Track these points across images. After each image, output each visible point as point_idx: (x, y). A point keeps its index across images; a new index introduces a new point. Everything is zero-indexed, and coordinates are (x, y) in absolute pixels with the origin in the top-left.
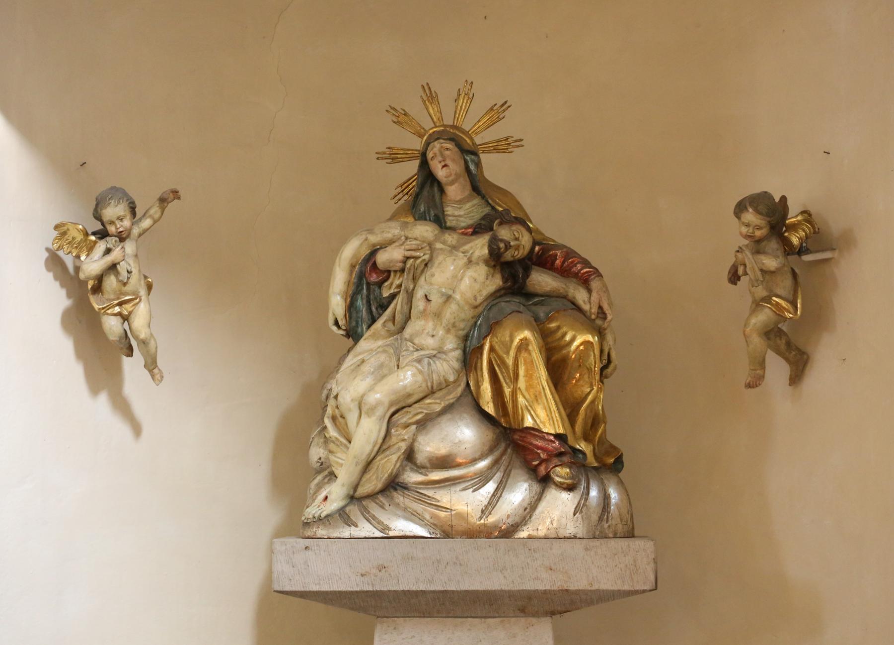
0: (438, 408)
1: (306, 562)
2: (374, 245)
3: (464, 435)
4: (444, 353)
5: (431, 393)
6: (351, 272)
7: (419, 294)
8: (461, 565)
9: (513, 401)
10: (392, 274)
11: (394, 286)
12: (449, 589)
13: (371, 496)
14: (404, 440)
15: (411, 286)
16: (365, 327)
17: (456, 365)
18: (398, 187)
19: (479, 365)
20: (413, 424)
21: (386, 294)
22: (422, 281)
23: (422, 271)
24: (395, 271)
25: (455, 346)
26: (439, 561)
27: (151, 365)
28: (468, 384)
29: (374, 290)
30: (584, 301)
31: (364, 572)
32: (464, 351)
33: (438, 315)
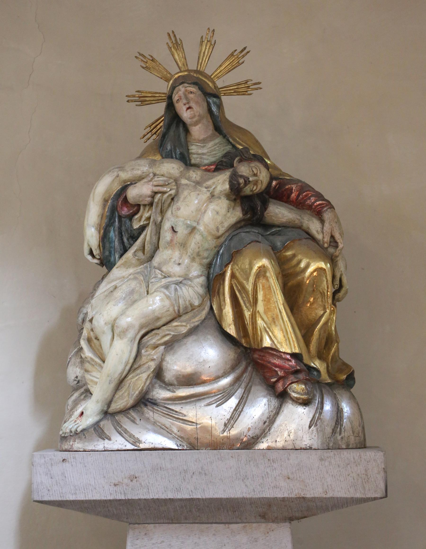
1: (63, 474)
2: (125, 181)
5: (178, 316)
6: (104, 206)
7: (167, 226)
8: (205, 474)
9: (253, 323)
10: (142, 208)
11: (143, 219)
13: (124, 411)
15: (159, 219)
16: (117, 256)
17: (201, 290)
21: (136, 226)
22: (169, 214)
23: (169, 205)
24: (145, 205)
26: (185, 471)
28: (211, 308)
30: (317, 231)
31: (116, 482)
32: (208, 278)
33: (183, 245)
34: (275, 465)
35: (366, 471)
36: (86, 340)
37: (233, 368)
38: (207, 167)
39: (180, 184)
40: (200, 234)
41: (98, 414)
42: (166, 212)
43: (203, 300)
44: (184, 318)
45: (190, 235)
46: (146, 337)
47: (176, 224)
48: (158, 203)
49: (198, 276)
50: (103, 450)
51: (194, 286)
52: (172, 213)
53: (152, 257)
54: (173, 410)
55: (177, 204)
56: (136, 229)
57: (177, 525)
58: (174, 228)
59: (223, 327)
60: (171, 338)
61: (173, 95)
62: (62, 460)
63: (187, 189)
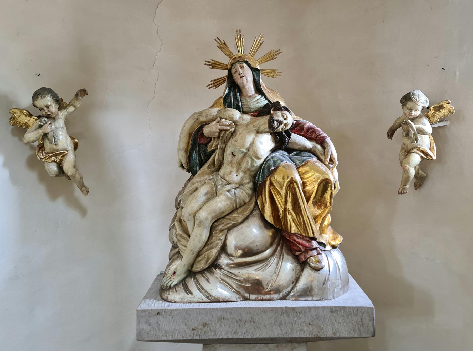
0: (240, 220)
1: (157, 323)
2: (202, 122)
3: (253, 233)
4: (242, 185)
5: (234, 210)
6: (190, 137)
7: (228, 151)
8: (254, 322)
9: (284, 219)
11: (214, 146)
12: (247, 337)
14: (220, 240)
15: (224, 146)
16: (198, 168)
17: (250, 192)
18: (212, 81)
19: (263, 192)
21: (209, 150)
22: (229, 143)
23: (230, 138)
24: (214, 138)
26: (241, 320)
27: (82, 187)
28: (256, 203)
29: (203, 148)
30: (321, 154)
31: (194, 328)
32: (254, 183)
33: (239, 164)
34: (301, 316)
35: (361, 319)
37: (271, 245)
41: (185, 273)
44: (239, 211)
46: (216, 223)
48: (223, 137)
49: (248, 183)
53: (219, 169)
54: (233, 274)
57: (234, 345)
61: (232, 69)
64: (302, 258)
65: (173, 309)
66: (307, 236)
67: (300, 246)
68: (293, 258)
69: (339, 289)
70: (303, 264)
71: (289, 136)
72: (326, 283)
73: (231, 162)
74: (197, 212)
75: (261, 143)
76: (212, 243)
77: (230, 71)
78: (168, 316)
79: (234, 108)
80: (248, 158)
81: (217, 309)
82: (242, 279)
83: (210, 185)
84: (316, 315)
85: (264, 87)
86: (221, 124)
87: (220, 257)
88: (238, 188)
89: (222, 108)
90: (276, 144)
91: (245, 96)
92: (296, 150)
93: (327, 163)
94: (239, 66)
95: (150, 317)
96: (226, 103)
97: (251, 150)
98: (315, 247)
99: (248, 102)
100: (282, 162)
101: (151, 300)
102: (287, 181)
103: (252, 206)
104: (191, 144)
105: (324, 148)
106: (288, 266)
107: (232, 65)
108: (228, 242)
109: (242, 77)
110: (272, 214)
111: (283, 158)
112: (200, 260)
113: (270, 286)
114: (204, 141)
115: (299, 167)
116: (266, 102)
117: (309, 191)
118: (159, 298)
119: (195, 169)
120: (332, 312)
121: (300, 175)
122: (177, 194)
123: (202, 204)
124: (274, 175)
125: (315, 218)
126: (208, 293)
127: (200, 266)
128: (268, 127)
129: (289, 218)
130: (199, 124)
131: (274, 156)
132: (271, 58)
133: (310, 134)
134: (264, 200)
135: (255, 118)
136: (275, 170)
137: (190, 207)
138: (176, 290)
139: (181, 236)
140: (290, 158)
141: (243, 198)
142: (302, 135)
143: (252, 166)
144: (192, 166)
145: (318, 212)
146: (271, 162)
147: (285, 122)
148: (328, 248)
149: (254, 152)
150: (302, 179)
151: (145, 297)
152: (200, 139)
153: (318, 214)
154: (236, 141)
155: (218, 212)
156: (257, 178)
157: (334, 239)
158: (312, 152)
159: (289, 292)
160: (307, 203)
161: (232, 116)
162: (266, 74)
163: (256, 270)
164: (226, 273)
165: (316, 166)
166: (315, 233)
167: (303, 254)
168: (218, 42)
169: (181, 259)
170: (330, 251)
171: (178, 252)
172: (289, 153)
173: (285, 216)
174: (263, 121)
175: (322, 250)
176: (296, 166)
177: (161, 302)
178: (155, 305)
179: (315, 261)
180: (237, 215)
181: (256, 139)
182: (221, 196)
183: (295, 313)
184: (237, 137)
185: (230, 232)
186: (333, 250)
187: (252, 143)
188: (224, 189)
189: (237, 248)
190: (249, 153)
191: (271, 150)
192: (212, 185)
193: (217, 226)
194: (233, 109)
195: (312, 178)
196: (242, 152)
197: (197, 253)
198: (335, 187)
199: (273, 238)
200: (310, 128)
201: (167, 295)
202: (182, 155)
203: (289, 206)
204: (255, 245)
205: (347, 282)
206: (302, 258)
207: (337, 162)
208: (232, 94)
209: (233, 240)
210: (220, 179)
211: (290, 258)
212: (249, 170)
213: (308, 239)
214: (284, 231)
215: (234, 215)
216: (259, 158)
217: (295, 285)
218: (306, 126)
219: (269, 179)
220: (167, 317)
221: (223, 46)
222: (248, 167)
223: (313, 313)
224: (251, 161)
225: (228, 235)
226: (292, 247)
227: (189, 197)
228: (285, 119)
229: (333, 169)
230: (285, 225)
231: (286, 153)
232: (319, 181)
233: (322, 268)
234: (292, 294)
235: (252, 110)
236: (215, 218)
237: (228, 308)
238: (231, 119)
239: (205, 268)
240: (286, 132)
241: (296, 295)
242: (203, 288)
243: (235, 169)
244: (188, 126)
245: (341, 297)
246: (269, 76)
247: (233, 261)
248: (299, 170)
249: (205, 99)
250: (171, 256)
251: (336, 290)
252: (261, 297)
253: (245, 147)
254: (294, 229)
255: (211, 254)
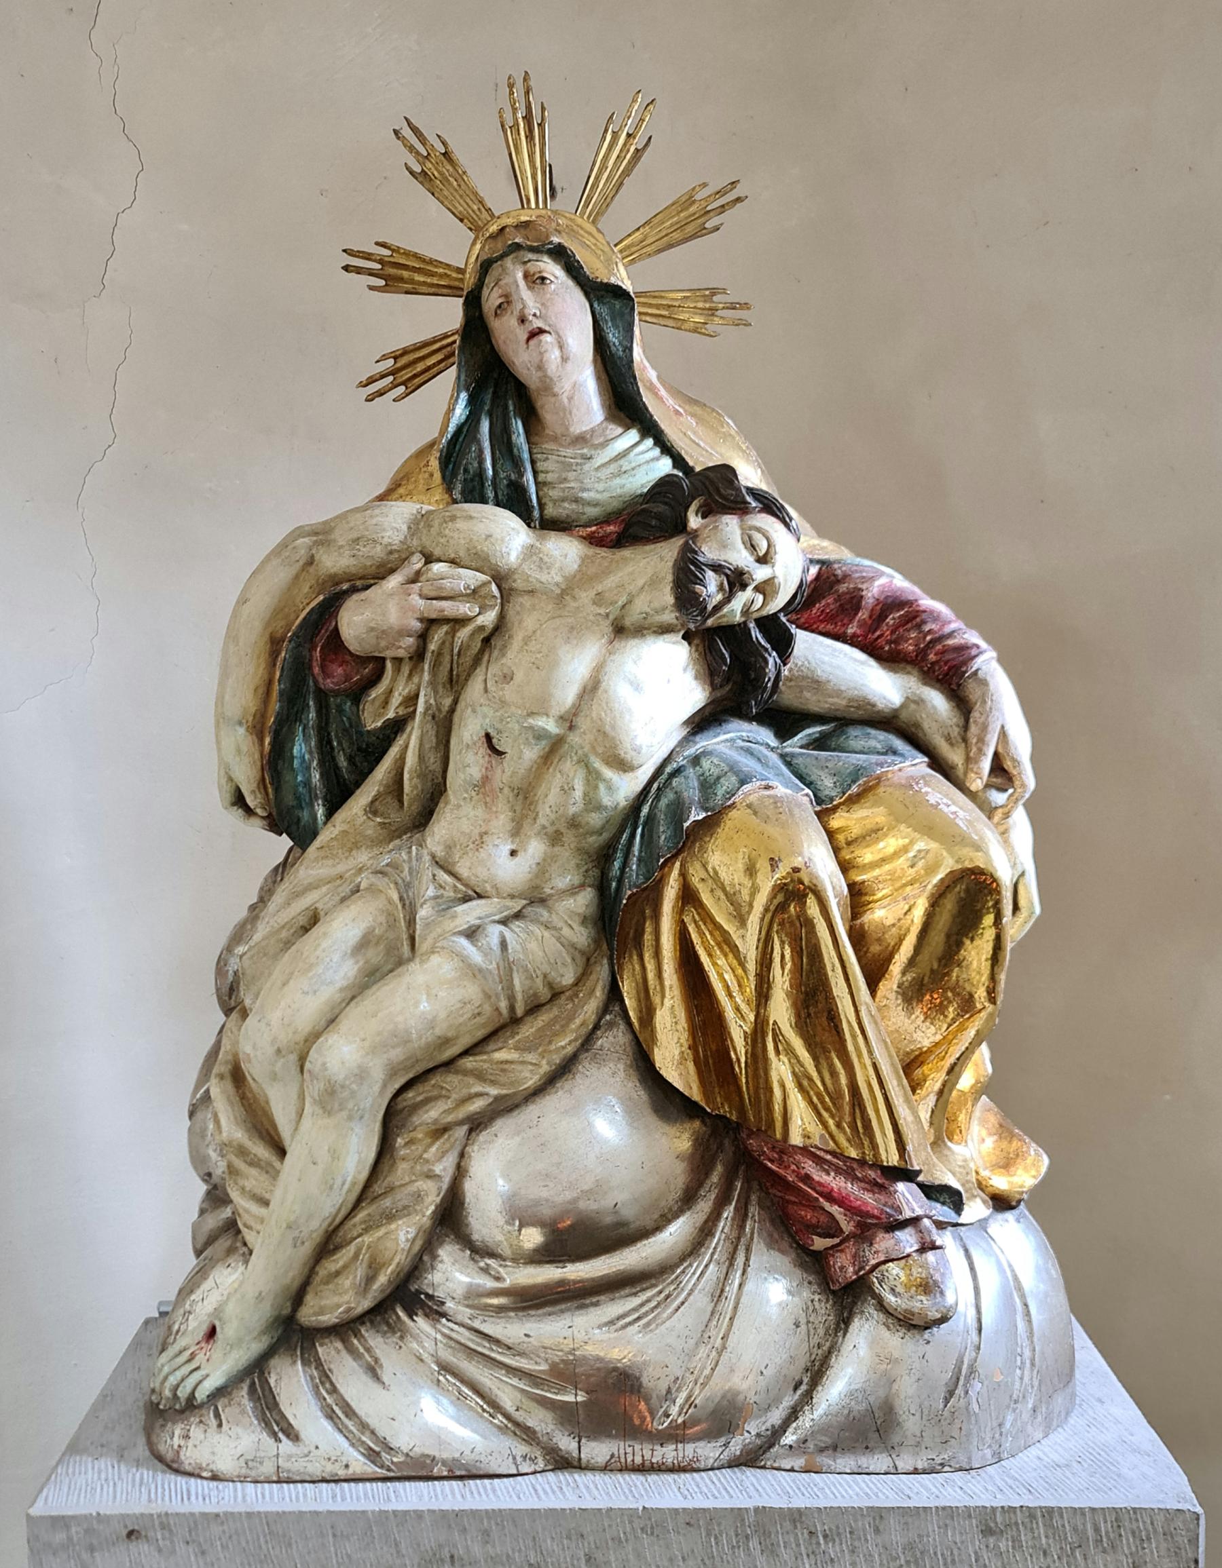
0: (531, 1080)
2: (335, 580)
4: (543, 901)
5: (503, 1027)
6: (274, 654)
7: (468, 730)
9: (756, 1076)
10: (389, 665)
11: (396, 700)
13: (345, 1330)
14: (430, 1176)
15: (447, 702)
16: (320, 812)
17: (581, 936)
18: (384, 358)
19: (648, 937)
20: (460, 1123)
21: (372, 722)
22: (474, 690)
23: (477, 661)
24: (398, 661)
25: (577, 880)
29: (340, 711)
30: (948, 739)
32: (602, 888)
33: (524, 796)
36: (228, 1075)
38: (594, 528)
39: (511, 589)
40: (579, 762)
41: (263, 1333)
42: (466, 680)
43: (588, 960)
44: (527, 1030)
45: (545, 763)
46: (410, 1094)
47: (498, 726)
48: (439, 654)
49: (573, 891)
50: (275, 1478)
51: (560, 924)
52: (486, 690)
53: (424, 818)
54: (497, 1342)
55: (504, 661)
56: (375, 729)
58: (494, 741)
59: (657, 1065)
60: (490, 1104)
61: (485, 292)
62: (125, 1533)
63: (533, 607)
64: (844, 1266)
65: (204, 1515)
66: (869, 1158)
67: (835, 1210)
68: (802, 1265)
69: (1026, 1416)
70: (847, 1297)
71: (784, 645)
72: (959, 1391)
73: (483, 785)
74: (314, 1037)
75: (637, 687)
76: (391, 1190)
77: (473, 302)
78: (181, 1548)
79: (498, 504)
80: (568, 766)
81: (419, 1515)
82: (544, 1367)
83: (380, 903)
84: (910, 1547)
85: (652, 388)
86: (429, 590)
87: (434, 1257)
88: (518, 916)
89: (432, 501)
90: (713, 687)
91: (555, 439)
92: (819, 719)
93: (976, 785)
94: (520, 275)
95: (92, 1549)
96: (454, 474)
97: (583, 723)
98: (908, 1214)
99: (568, 467)
100: (743, 782)
101: (102, 1463)
102: (766, 884)
103: (591, 1008)
104: (281, 693)
105: (963, 704)
106: (774, 1294)
107: (485, 267)
108: (470, 1187)
109: (536, 333)
110: (693, 1047)
111: (747, 764)
112: (338, 1273)
113: (679, 1401)
114: (347, 678)
115: (835, 809)
116: (665, 466)
117: (885, 929)
118: (141, 1450)
119: (305, 815)
120: (987, 1531)
121: (836, 850)
122: (222, 941)
123: (338, 997)
124: (703, 850)
125: (912, 1065)
126: (373, 1432)
127: (336, 1299)
128: (671, 600)
129: (780, 1070)
130: (321, 585)
131: (705, 753)
132: (690, 229)
133: (890, 634)
134: (651, 975)
135: (603, 552)
136: (709, 825)
137: (278, 1014)
138: (217, 1415)
139: (242, 1152)
140: (788, 760)
141: (546, 968)
142: (852, 641)
143: (592, 803)
144: (289, 800)
145: (924, 1033)
146: (688, 786)
147: (761, 573)
148: (975, 1209)
149: (602, 732)
150: (845, 867)
151: (74, 1448)
152: (323, 667)
153: (926, 1044)
154: (508, 678)
155: (421, 1038)
156: (617, 864)
157: (1006, 1164)
158: (901, 727)
159: (777, 1432)
160: (873, 985)
161: (485, 547)
162: (667, 315)
163: (611, 1323)
164: (464, 1336)
165: (919, 801)
166: (910, 1148)
167: (851, 1247)
168: (411, 149)
169: (246, 1262)
170: (983, 1224)
171: (232, 1227)
172: (784, 733)
173: (758, 1059)
174: (647, 570)
175: (940, 1225)
176: (819, 801)
177: (147, 1474)
178: (111, 1489)
179: (907, 1287)
180: (514, 1055)
181: (611, 667)
182: (435, 960)
183: (803, 1535)
184: (513, 656)
185: (483, 1136)
186: (1000, 1216)
187: (592, 688)
188: (450, 925)
189: (521, 1216)
190: (574, 738)
191: (687, 722)
192: (390, 901)
193: (415, 1108)
194: (490, 510)
195: (902, 862)
196: (540, 735)
197: (317, 1237)
198: (1016, 908)
199: (700, 1164)
200: (891, 603)
201: (176, 1441)
202: (239, 751)
203: (781, 1010)
204: (608, 1202)
205: (1065, 1372)
206: (844, 1266)
207: (1029, 779)
208: (485, 426)
209: (498, 1176)
210: (427, 869)
211: (783, 1261)
212: (574, 823)
213: (872, 1174)
214: (751, 1134)
215: (498, 1056)
216: (623, 766)
217: (808, 1397)
218: (873, 592)
219: (675, 873)
220: (173, 1552)
221: (436, 170)
222: (572, 810)
223: (896, 1536)
224: (588, 782)
225: (474, 1151)
226: (791, 1209)
227: (276, 957)
228: (763, 560)
229: (1007, 815)
230: (756, 1101)
231: (766, 735)
232: (936, 879)
233: (944, 1319)
234: (789, 1438)
235: (592, 512)
236: (406, 1069)
237: (474, 1513)
238: (480, 562)
239: (360, 1310)
240: (769, 624)
241: (811, 1445)
242: (349, 1412)
243: (502, 821)
244: (262, 602)
245: (1033, 1451)
246: (679, 325)
247: (498, 1279)
248: (835, 822)
249: (348, 461)
250: (201, 1240)
251: (1010, 1417)
252: (641, 1452)
253: (556, 711)
254: (801, 1123)
255: (389, 1244)
